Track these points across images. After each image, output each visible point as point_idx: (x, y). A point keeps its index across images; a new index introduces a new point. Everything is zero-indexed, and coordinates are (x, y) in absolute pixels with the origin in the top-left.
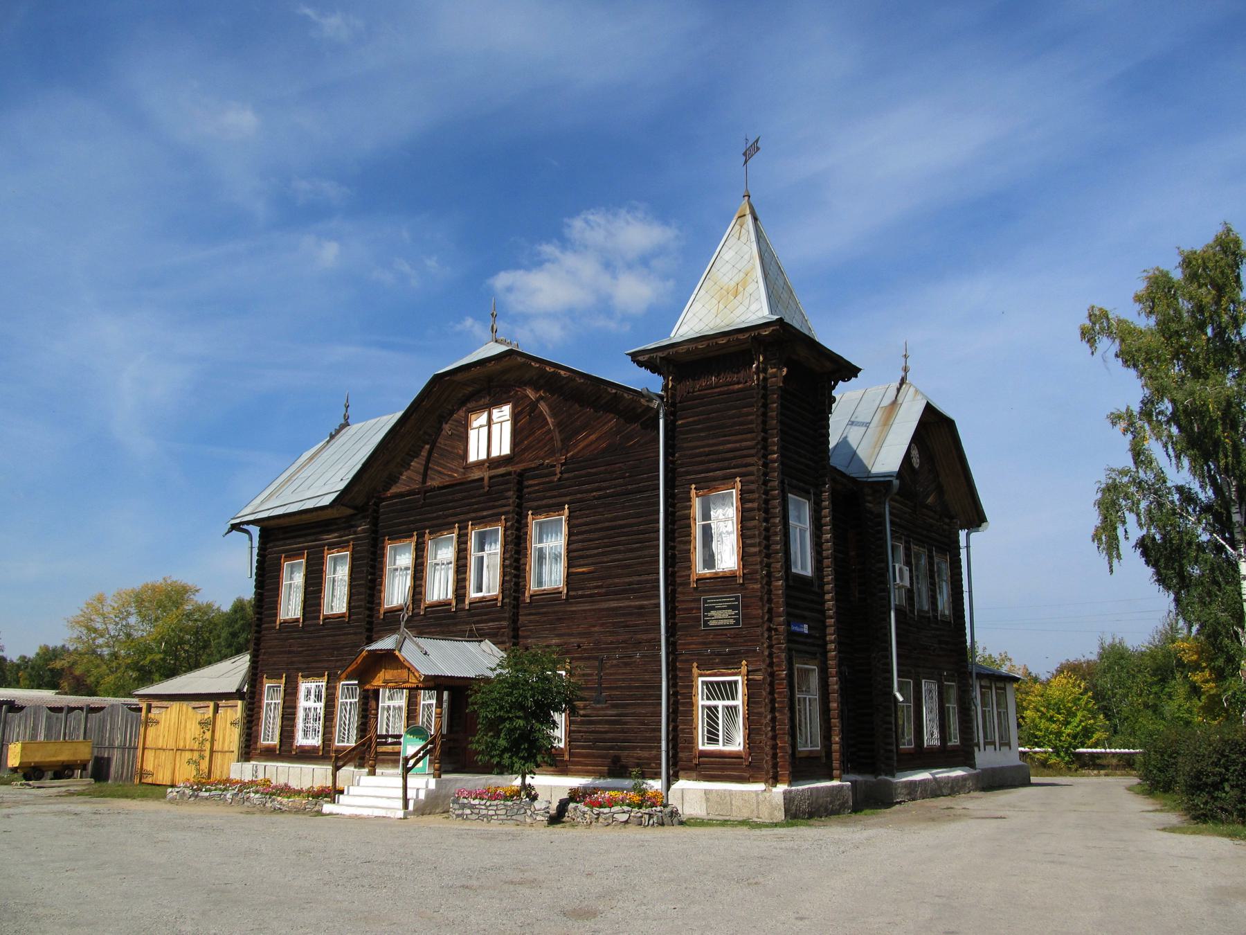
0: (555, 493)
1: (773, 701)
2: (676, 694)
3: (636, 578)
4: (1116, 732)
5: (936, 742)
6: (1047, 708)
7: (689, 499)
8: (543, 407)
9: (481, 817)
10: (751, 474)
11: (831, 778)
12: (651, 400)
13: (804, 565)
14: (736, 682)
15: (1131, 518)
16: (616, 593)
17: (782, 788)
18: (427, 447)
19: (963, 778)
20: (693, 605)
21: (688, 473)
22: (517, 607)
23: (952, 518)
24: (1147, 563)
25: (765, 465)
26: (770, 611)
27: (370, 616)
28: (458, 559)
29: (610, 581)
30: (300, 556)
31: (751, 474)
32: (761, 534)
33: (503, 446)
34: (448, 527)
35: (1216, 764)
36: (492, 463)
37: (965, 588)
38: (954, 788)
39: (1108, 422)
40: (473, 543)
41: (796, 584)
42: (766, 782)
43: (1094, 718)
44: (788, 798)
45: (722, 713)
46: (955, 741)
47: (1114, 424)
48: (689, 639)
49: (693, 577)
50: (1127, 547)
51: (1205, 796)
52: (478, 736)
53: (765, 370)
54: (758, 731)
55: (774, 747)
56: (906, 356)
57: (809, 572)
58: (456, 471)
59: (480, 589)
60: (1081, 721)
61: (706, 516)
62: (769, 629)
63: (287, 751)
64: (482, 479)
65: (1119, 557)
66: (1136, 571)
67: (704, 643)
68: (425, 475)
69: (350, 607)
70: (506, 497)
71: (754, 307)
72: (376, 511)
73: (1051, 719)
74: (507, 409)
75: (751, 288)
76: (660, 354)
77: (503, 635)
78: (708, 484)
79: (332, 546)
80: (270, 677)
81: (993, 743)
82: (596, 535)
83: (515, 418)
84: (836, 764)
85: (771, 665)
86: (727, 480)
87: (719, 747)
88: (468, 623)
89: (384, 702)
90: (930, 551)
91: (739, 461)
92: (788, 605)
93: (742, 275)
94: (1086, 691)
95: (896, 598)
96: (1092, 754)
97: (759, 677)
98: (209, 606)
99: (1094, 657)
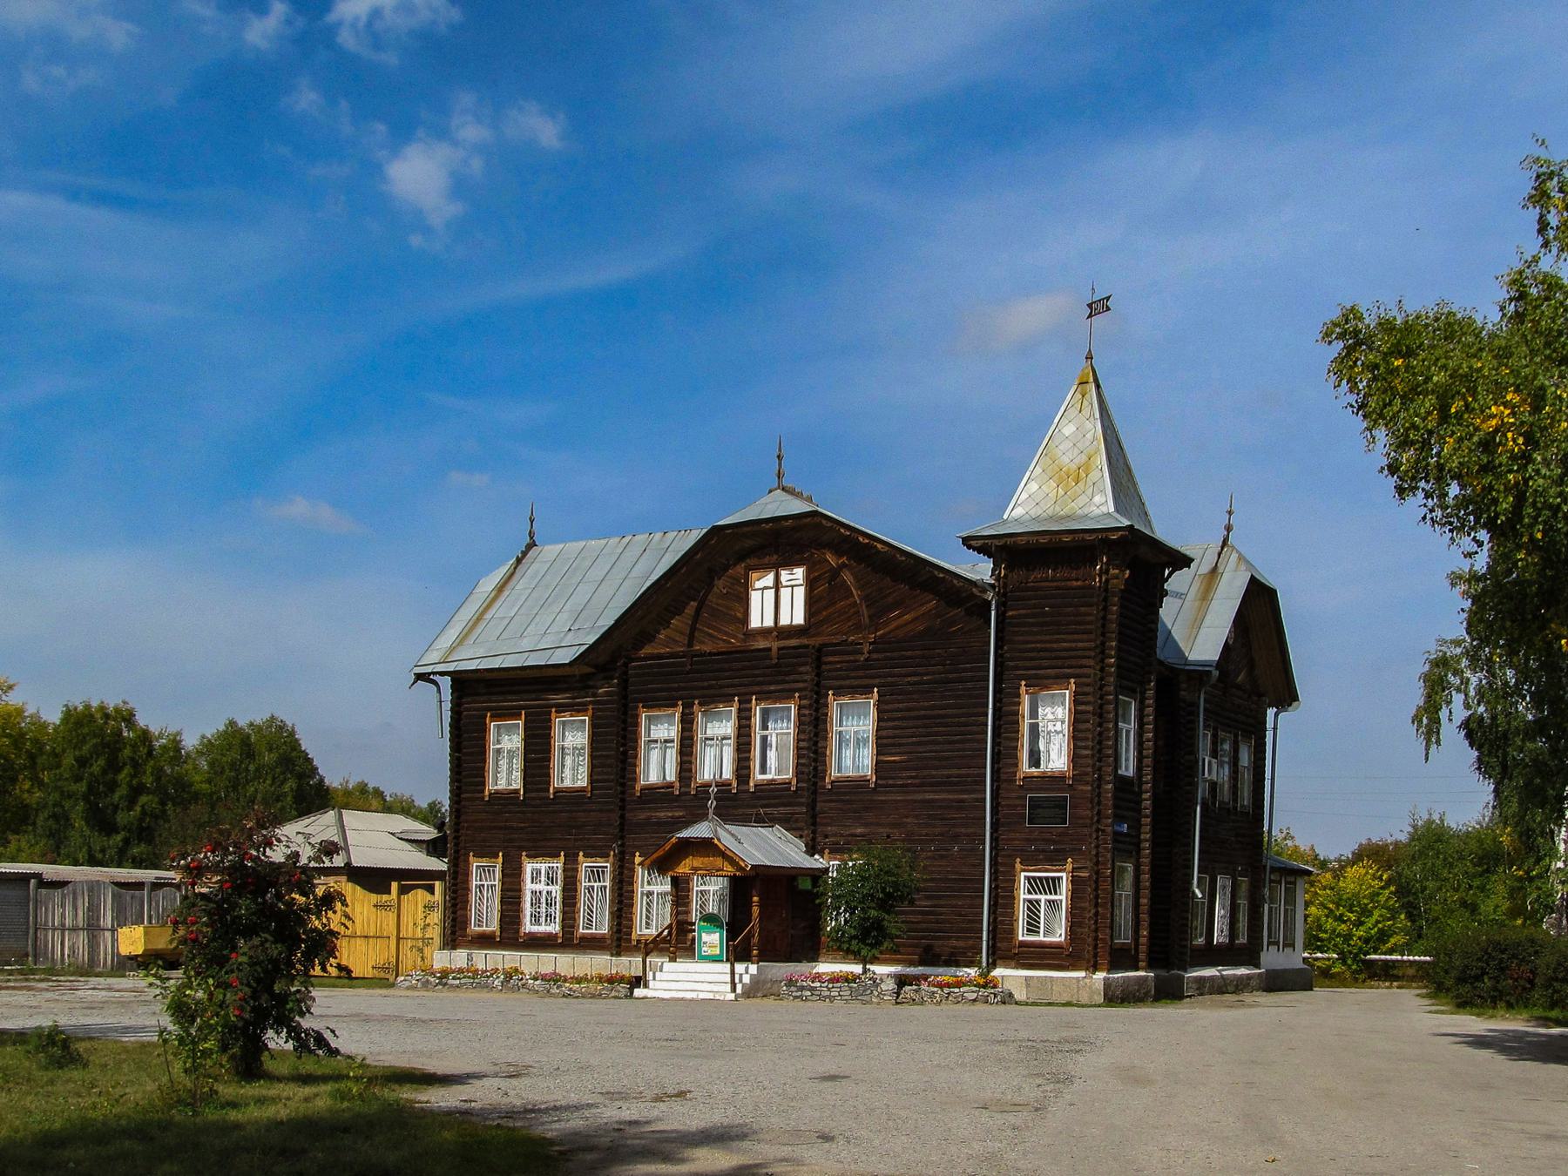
0: (861, 673)
1: (1097, 897)
2: (997, 887)
3: (955, 771)
4: (1420, 936)
5: (1224, 940)
6: (1338, 905)
7: (1019, 696)
8: (847, 577)
9: (822, 998)
10: (1088, 676)
11: (1137, 969)
12: (984, 591)
13: (1128, 768)
14: (1059, 878)
15: (1458, 699)
16: (932, 785)
17: (1100, 975)
18: (694, 604)
19: (1249, 977)
20: (1018, 802)
21: (1018, 668)
22: (815, 792)
23: (1260, 695)
24: (1471, 745)
25: (1102, 670)
26: (1099, 813)
27: (623, 793)
28: (739, 736)
29: (926, 772)
30: (518, 716)
31: (1088, 676)
32: (1090, 734)
33: (794, 612)
34: (728, 700)
35: (1479, 960)
36: (779, 632)
37: (1268, 775)
38: (1240, 986)
39: (1447, 583)
40: (757, 720)
41: (1123, 783)
42: (1087, 969)
43: (1393, 918)
44: (1107, 984)
45: (1045, 905)
46: (1242, 940)
47: (1453, 585)
48: (1012, 835)
49: (1020, 775)
50: (1451, 733)
51: (1468, 987)
52: (775, 921)
53: (1107, 572)
54: (1080, 925)
55: (1096, 938)
56: (1230, 513)
57: (1131, 773)
58: (734, 637)
59: (763, 770)
60: (1378, 922)
61: (1034, 714)
62: (1098, 830)
63: (510, 936)
64: (769, 649)
65: (1438, 742)
66: (1457, 751)
67: (1028, 840)
68: (691, 638)
69: (592, 780)
70: (799, 671)
71: (1098, 499)
72: (626, 673)
73: (1340, 919)
74: (799, 572)
75: (1094, 476)
76: (996, 542)
77: (797, 821)
78: (1040, 683)
79: (562, 708)
80: (479, 855)
81: (1277, 943)
82: (911, 723)
83: (811, 584)
84: (1142, 956)
85: (1097, 863)
86: (1060, 680)
87: (1041, 938)
88: (755, 806)
89: (697, 886)
90: (1236, 736)
91: (1073, 662)
92: (1116, 807)
93: (1084, 458)
94: (1389, 882)
95: (1202, 792)
96: (1386, 961)
97: (1085, 874)
98: (20, 712)
99: (1403, 838)
